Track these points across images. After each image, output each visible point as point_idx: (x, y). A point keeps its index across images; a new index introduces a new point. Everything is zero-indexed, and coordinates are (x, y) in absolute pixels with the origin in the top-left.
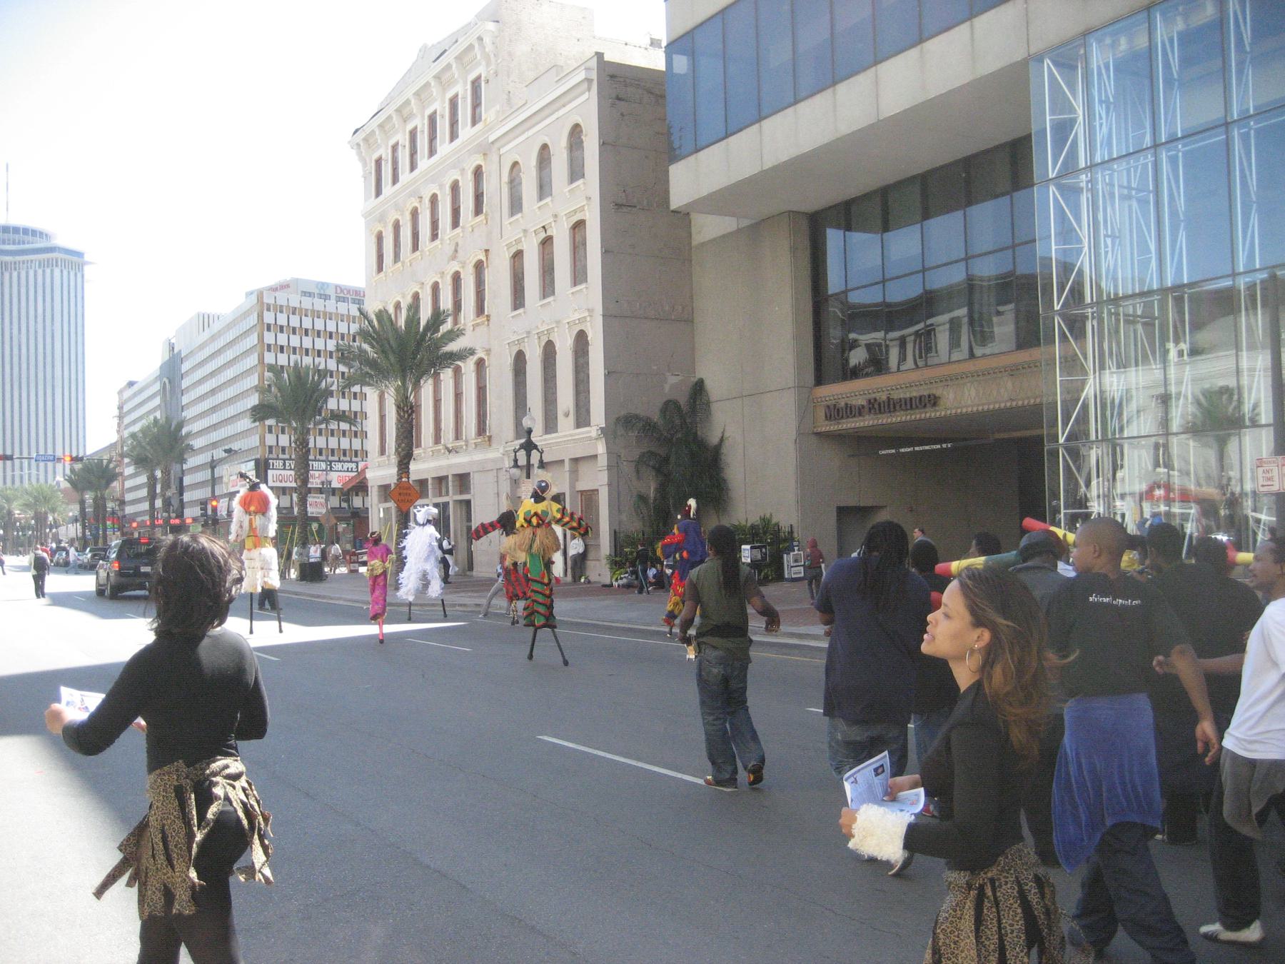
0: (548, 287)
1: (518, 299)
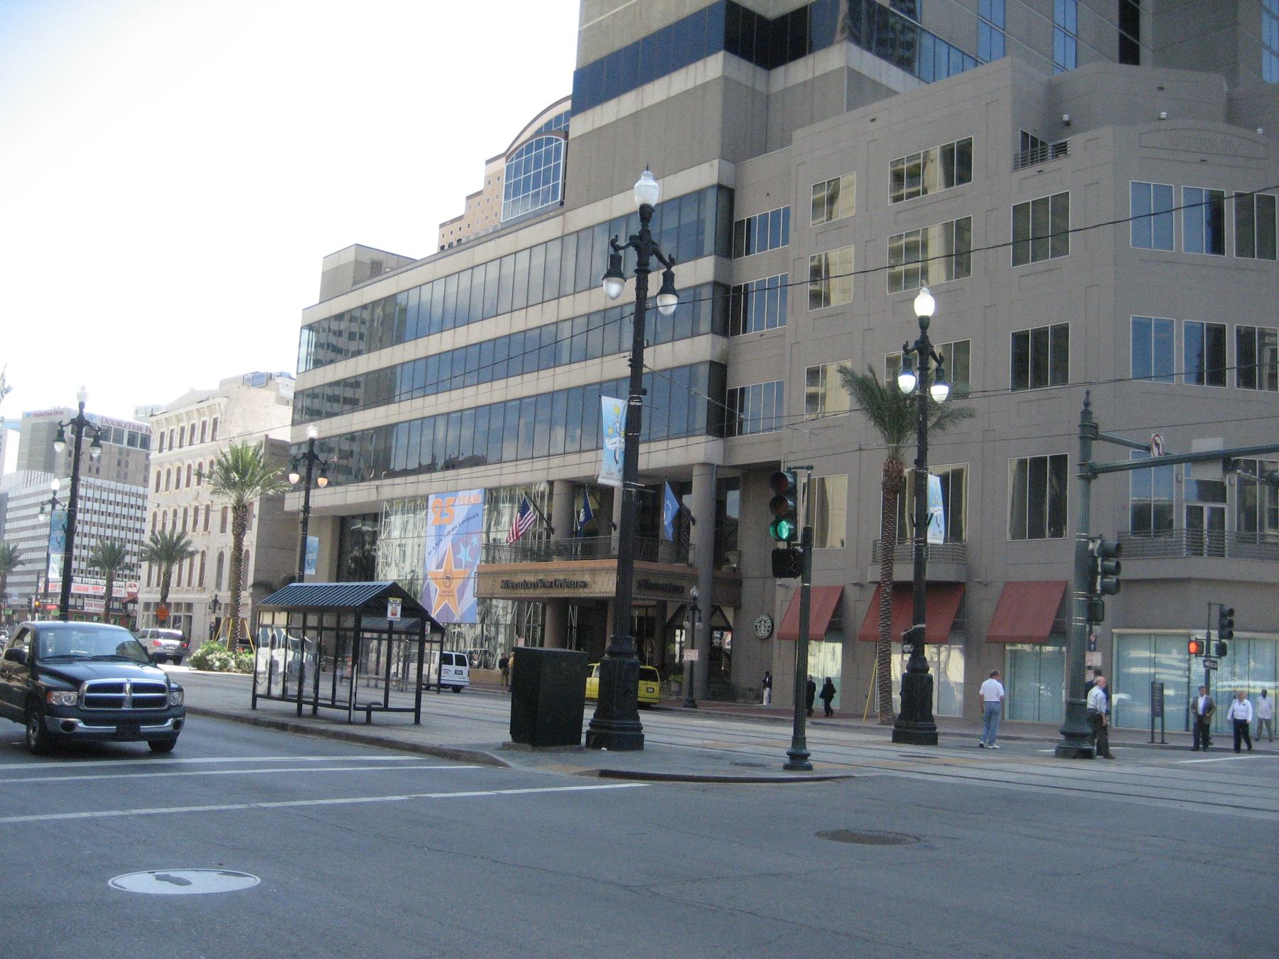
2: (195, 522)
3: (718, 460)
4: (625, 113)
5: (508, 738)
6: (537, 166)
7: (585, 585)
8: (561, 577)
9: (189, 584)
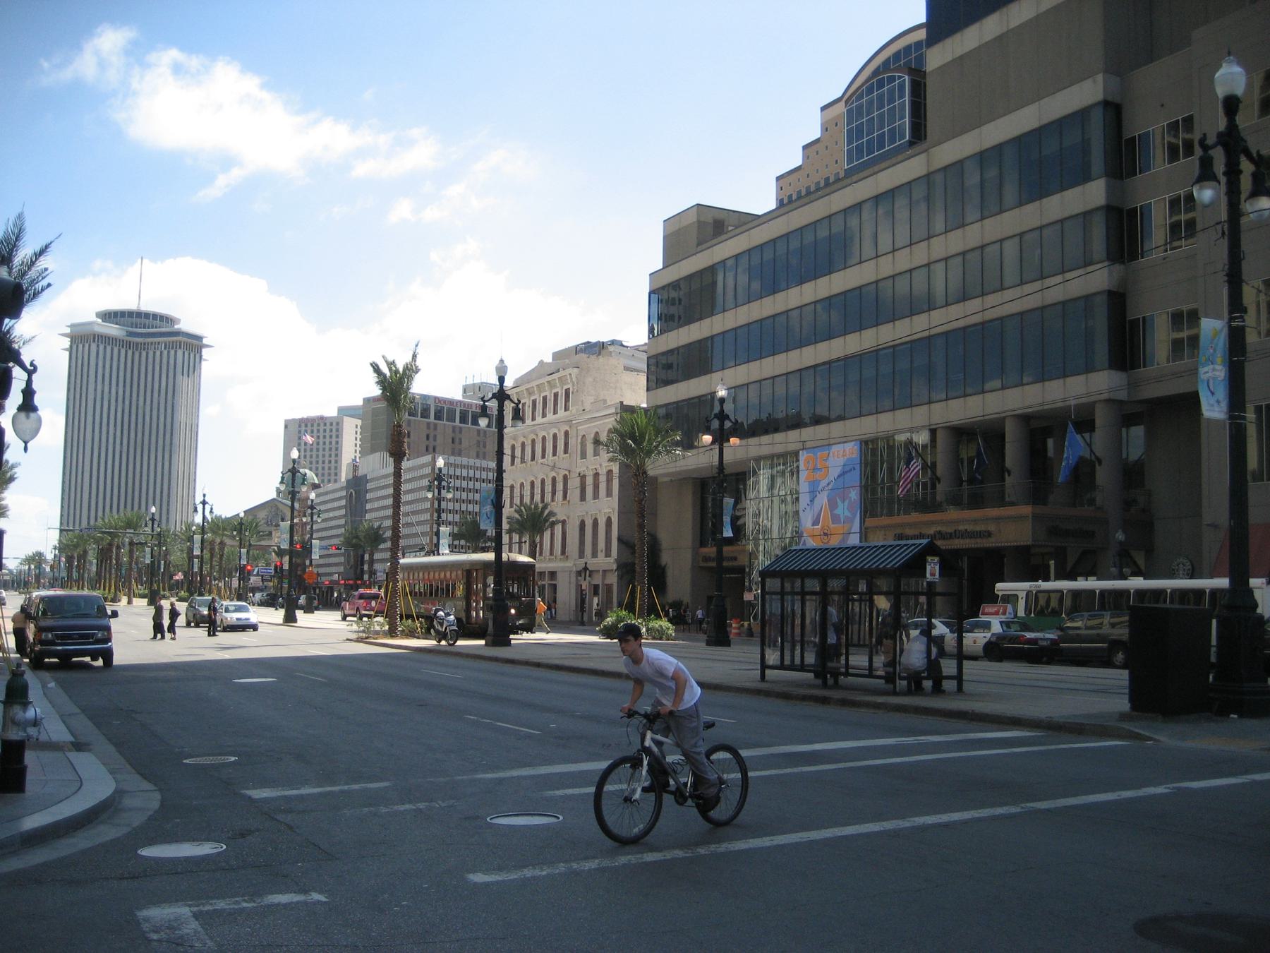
0: (596, 496)
1: (583, 498)
2: (554, 492)
3: (1123, 395)
4: (988, 37)
5: (1124, 704)
6: (881, 106)
7: (989, 534)
8: (961, 528)
9: (551, 554)
